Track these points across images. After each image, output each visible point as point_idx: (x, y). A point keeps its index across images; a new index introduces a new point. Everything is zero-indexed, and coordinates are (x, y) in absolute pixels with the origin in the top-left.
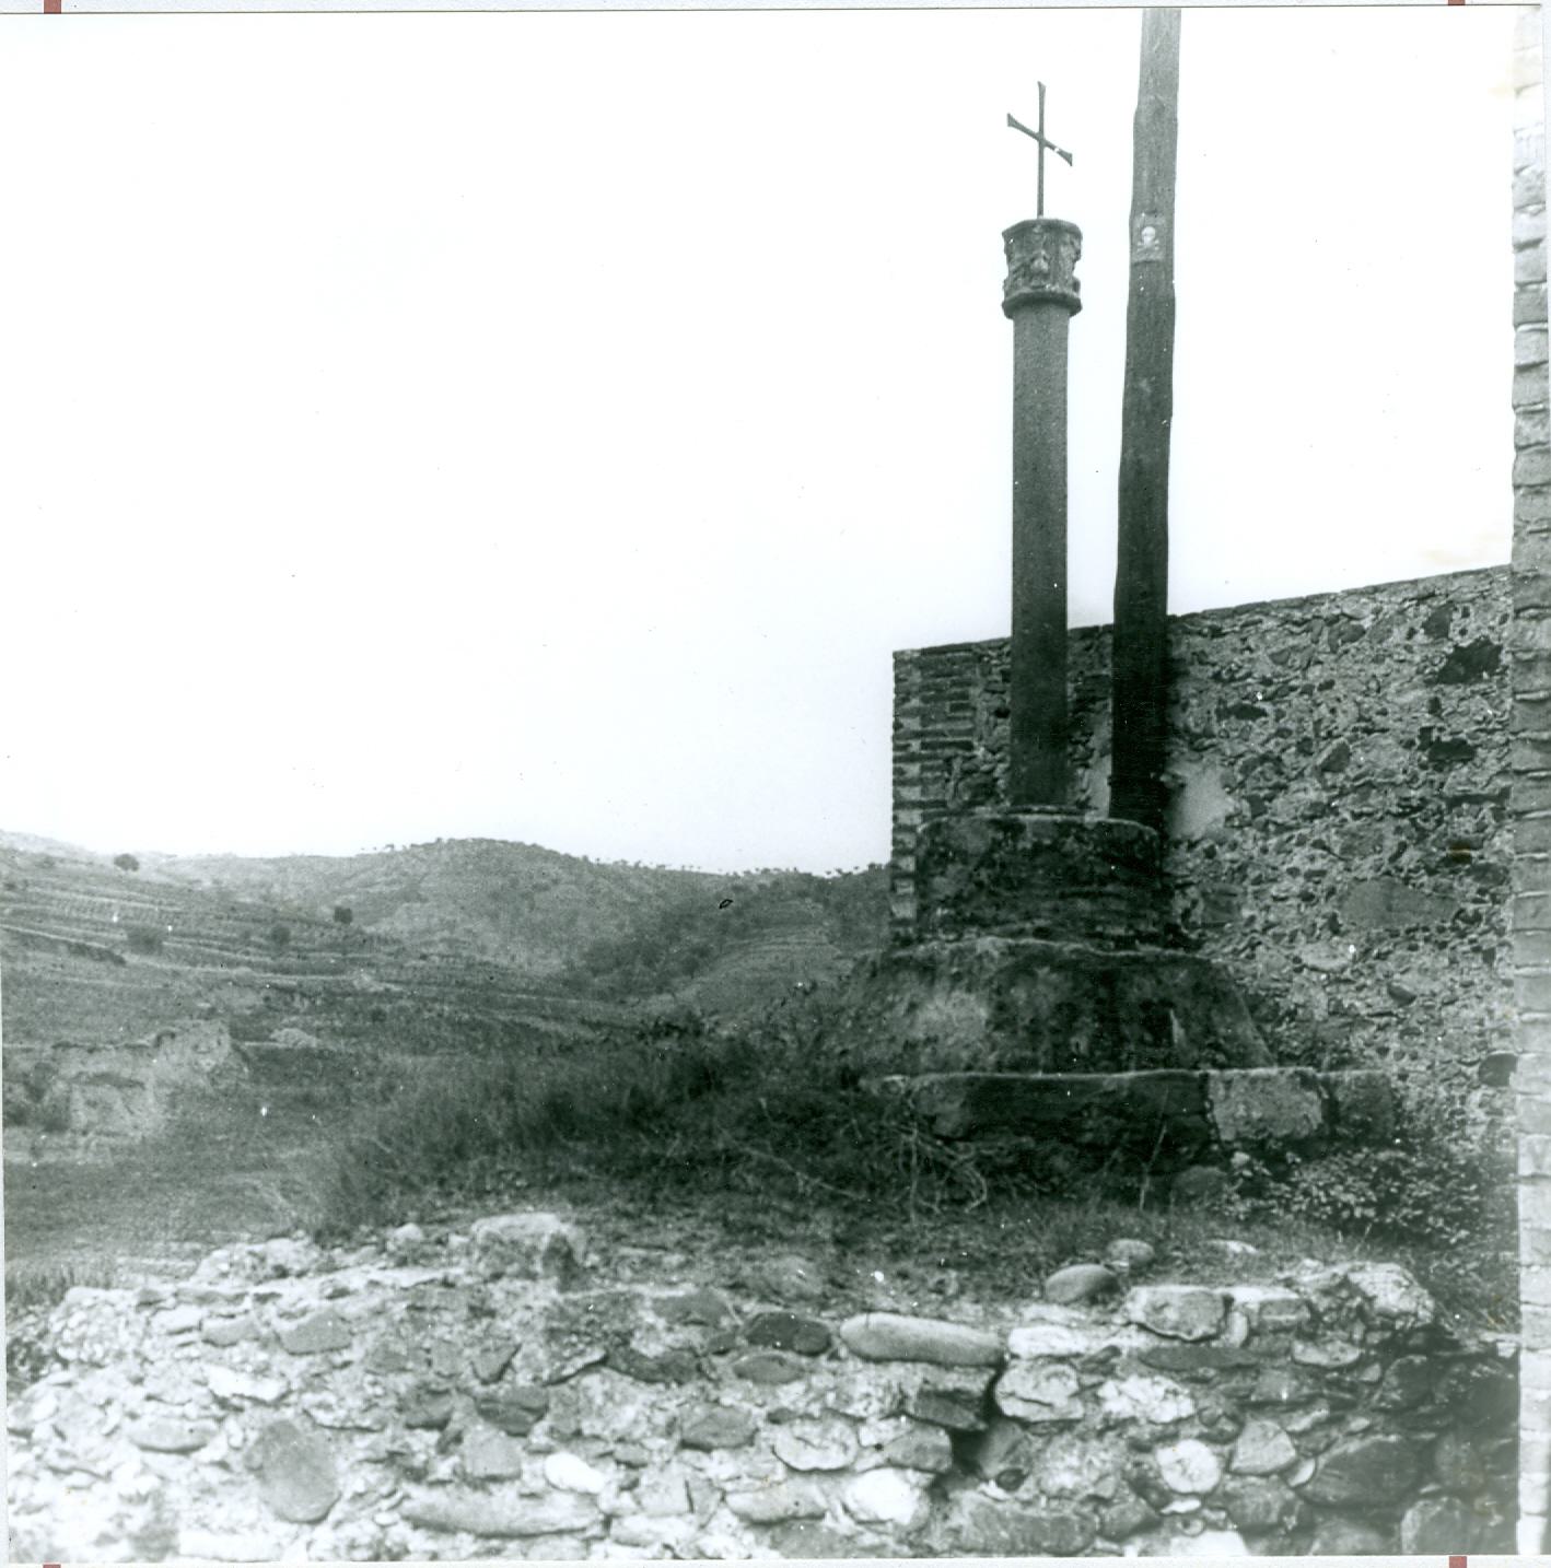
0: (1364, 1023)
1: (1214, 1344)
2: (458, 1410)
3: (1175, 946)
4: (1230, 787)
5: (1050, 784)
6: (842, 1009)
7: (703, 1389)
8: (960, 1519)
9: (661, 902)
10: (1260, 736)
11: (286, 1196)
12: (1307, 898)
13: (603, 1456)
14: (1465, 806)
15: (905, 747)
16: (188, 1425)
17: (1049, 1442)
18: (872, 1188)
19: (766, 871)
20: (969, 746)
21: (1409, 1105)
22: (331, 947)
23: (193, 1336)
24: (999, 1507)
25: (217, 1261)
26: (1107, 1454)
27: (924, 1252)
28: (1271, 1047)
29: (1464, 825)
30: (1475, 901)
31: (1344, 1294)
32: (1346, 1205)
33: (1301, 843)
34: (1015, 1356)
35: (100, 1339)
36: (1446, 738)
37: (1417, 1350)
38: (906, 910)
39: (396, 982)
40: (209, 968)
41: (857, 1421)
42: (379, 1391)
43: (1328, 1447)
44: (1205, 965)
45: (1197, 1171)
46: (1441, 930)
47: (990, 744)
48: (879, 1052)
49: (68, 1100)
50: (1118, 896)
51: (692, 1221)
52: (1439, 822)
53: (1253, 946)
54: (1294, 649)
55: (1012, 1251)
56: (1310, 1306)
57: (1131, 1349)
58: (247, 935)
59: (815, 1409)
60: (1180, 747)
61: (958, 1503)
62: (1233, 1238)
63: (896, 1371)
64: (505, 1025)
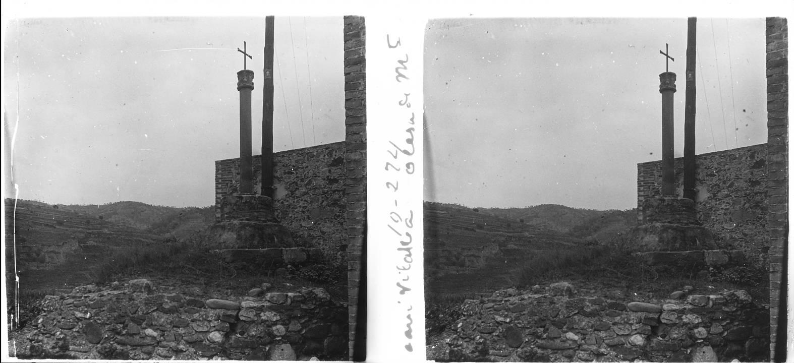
0: (737, 240)
1: (284, 305)
2: (127, 320)
3: (697, 225)
4: (709, 191)
5: (249, 189)
6: (206, 236)
7: (599, 318)
8: (653, 344)
9: (589, 217)
10: (715, 180)
11: (511, 279)
12: (725, 214)
13: (157, 329)
14: (758, 194)
15: (218, 181)
16: (71, 324)
17: (671, 328)
18: (212, 273)
19: (611, 210)
20: (231, 181)
21: (325, 255)
22: (99, 224)
23: (492, 309)
24: (661, 342)
25: (76, 289)
26: (683, 331)
27: (224, 286)
28: (296, 243)
29: (758, 198)
30: (339, 212)
31: (733, 296)
32: (312, 276)
33: (724, 202)
34: (242, 307)
35: (52, 306)
36: (332, 178)
37: (326, 306)
38: (219, 215)
39: (534, 234)
40: (494, 232)
41: (631, 324)
42: (531, 320)
43: (308, 326)
44: (704, 229)
45: (702, 272)
46: (332, 218)
47: (236, 180)
48: (635, 248)
49: (464, 260)
50: (263, 212)
51: (596, 283)
52: (331, 196)
53: (292, 222)
54: (300, 159)
55: (663, 288)
56: (304, 296)
57: (689, 308)
58: (502, 225)
59: (622, 322)
60: (276, 180)
61: (652, 341)
62: (288, 283)
63: (639, 314)
64: (135, 240)
